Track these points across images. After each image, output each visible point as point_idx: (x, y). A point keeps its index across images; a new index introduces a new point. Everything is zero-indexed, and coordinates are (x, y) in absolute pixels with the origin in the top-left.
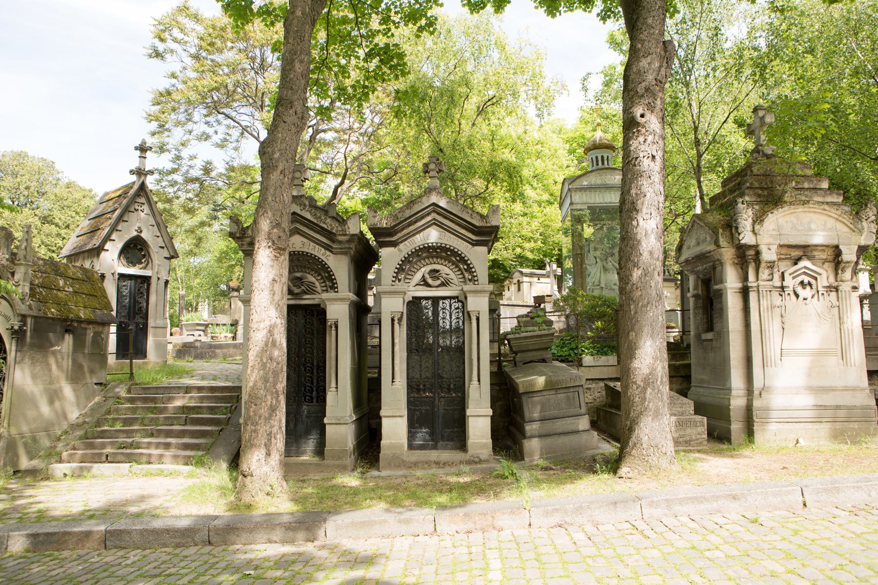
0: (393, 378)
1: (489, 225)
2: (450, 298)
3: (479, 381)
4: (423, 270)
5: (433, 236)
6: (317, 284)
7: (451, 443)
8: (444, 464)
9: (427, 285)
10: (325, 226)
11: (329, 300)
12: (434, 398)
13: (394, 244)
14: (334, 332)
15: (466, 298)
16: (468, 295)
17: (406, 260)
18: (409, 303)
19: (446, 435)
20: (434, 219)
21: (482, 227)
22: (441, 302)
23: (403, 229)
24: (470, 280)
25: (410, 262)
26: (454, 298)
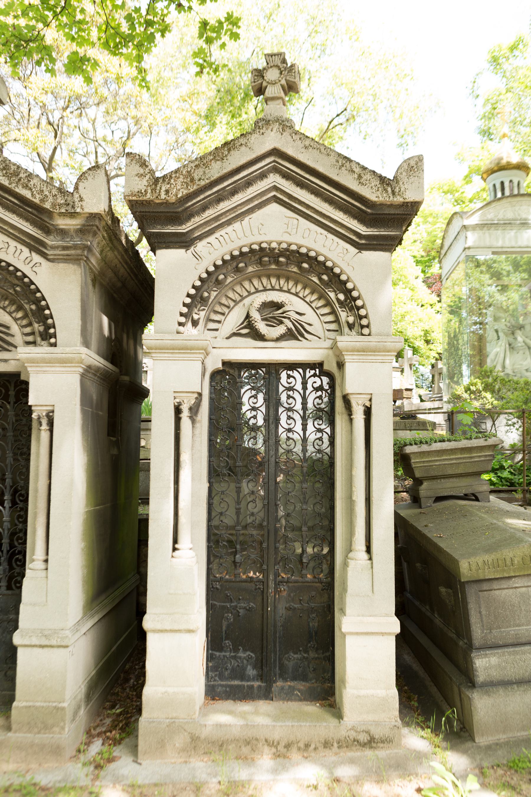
0: (175, 541)
1: (398, 200)
2: (305, 366)
3: (369, 550)
4: (247, 301)
5: (274, 227)
6: (15, 329)
7: (301, 685)
8: (288, 746)
9: (258, 336)
10: (27, 194)
11: (33, 361)
12: (264, 583)
13: (184, 242)
14: (45, 435)
15: (341, 365)
16: (348, 358)
17: (211, 279)
18: (215, 374)
19: (290, 665)
20: (275, 188)
21: (382, 205)
22: (284, 375)
23: (204, 208)
24: (351, 326)
25: (218, 282)
26: (312, 366)
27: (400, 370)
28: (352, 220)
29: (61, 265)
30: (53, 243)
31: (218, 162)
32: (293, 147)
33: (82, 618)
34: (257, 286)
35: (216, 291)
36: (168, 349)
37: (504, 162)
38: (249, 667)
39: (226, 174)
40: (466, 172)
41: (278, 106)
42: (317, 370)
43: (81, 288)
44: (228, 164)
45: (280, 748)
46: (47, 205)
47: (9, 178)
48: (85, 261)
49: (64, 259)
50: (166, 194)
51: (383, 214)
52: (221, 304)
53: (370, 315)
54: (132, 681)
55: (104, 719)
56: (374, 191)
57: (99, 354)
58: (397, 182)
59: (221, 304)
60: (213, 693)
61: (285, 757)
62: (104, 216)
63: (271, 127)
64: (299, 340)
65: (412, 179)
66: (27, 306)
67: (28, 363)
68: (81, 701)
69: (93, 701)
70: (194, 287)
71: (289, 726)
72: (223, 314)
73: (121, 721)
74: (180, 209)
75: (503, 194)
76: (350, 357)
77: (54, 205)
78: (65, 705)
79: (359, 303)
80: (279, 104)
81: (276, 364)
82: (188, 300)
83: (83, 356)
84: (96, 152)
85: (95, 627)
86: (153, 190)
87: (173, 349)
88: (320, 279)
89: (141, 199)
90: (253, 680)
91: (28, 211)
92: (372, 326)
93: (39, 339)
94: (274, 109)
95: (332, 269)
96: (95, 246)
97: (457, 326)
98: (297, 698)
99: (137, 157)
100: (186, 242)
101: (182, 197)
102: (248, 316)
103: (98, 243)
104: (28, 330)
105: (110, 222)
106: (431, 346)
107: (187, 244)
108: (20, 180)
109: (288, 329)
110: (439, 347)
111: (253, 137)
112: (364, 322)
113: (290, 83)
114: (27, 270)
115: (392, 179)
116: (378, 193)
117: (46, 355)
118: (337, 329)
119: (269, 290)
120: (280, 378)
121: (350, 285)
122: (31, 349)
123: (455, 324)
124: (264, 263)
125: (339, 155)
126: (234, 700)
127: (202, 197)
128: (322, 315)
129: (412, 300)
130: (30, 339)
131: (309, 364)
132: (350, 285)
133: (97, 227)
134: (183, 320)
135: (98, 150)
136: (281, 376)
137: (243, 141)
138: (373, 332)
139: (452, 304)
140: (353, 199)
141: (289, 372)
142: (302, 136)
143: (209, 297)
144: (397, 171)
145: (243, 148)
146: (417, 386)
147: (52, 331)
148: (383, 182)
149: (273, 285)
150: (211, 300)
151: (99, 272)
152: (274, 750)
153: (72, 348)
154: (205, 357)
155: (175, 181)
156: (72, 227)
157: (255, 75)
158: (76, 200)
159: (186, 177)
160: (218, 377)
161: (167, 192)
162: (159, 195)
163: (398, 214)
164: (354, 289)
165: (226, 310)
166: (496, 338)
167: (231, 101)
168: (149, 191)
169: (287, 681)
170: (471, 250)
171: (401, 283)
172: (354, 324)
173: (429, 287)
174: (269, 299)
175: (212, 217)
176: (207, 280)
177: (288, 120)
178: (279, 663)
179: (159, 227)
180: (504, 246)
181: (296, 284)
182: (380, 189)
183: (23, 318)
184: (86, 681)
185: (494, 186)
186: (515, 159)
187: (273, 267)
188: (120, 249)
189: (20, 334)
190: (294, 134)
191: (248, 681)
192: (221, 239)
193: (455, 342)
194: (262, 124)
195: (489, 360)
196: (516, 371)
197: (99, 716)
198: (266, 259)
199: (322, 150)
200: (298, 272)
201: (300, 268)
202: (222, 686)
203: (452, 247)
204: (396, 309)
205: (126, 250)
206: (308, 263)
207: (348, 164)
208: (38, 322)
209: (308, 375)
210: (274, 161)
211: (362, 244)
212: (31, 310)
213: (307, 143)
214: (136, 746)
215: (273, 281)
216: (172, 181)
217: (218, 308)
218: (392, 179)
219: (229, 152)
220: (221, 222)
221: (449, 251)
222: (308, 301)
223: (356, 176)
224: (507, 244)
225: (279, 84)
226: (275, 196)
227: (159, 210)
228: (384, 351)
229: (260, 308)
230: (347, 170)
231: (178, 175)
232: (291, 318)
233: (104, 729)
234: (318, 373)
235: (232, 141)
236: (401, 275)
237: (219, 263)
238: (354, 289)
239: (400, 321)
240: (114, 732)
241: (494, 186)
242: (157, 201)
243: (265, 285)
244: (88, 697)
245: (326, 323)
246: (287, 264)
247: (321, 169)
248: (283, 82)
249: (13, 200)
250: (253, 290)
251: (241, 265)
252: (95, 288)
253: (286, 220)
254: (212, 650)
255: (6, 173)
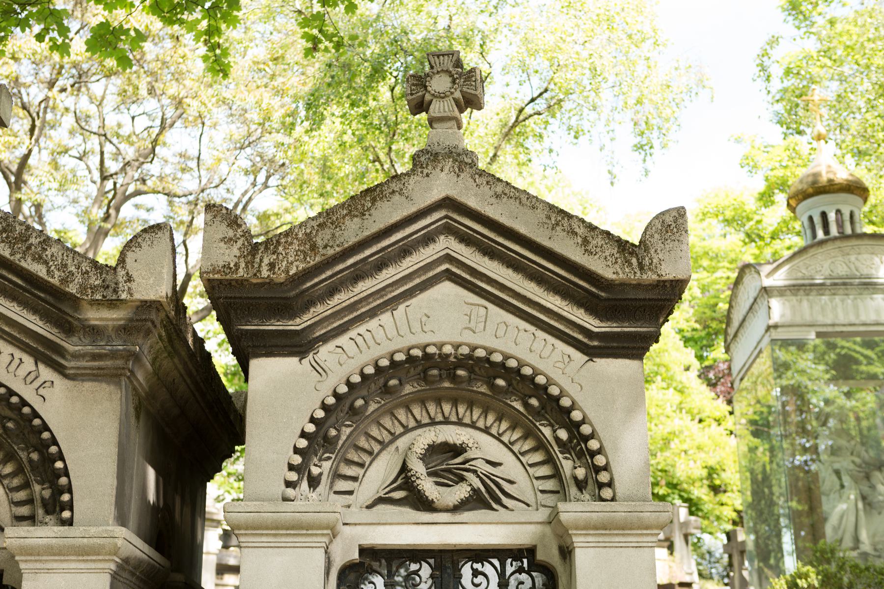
1: (650, 277)
2: (501, 553)
4: (402, 443)
5: (445, 318)
9: (421, 502)
10: (39, 270)
11: (31, 552)
13: (298, 345)
15: (566, 553)
16: (578, 540)
17: (342, 407)
21: (623, 285)
22: (466, 571)
23: (332, 291)
24: (581, 485)
25: (353, 412)
27: (667, 544)
28: (575, 308)
29: (88, 385)
30: (77, 348)
31: (355, 219)
32: (476, 195)
34: (418, 417)
35: (349, 426)
36: (267, 528)
37: (824, 179)
39: (368, 237)
40: (762, 187)
41: (450, 131)
42: (525, 561)
43: (120, 424)
44: (371, 222)
46: (72, 289)
47: (11, 246)
48: (129, 378)
49: (94, 375)
50: (270, 270)
51: (625, 300)
52: (358, 448)
53: (613, 466)
56: (609, 263)
57: (139, 535)
58: (647, 250)
59: (358, 448)
62: (165, 305)
63: (441, 165)
64: (493, 509)
65: (670, 245)
66: (23, 455)
67: (21, 555)
70: (312, 420)
72: (361, 465)
74: (292, 294)
75: (827, 232)
76: (582, 539)
77: (83, 288)
79: (594, 444)
80: (451, 128)
81: (452, 551)
82: (303, 443)
83: (120, 542)
84: (102, 153)
86: (249, 264)
87: (277, 528)
88: (526, 405)
89: (228, 277)
91: (39, 298)
92: (617, 484)
93: (40, 512)
94: (444, 134)
95: (545, 388)
96: (146, 353)
97: (767, 459)
99: (224, 211)
100: (301, 346)
101: (295, 274)
102: (404, 468)
103: (151, 347)
104: (21, 495)
105: (173, 313)
106: (723, 497)
107: (302, 349)
108: (29, 248)
109: (473, 489)
110: (736, 500)
111: (413, 180)
112: (604, 477)
113: (467, 96)
114: (28, 393)
115: (637, 244)
116: (617, 266)
117: (54, 541)
118: (558, 488)
119: (440, 423)
120: (460, 577)
121: (576, 415)
122: (24, 530)
123: (763, 455)
124: (431, 379)
125: (552, 207)
127: (329, 273)
128: (531, 465)
129: (681, 409)
130: (24, 511)
131: (511, 550)
132: (576, 415)
133: (153, 322)
134: (293, 476)
135: (106, 150)
136: (463, 571)
137: (395, 186)
138: (619, 495)
139: (757, 418)
140: (576, 275)
141: (475, 566)
142: (490, 179)
143: (338, 437)
144: (645, 232)
145: (396, 198)
146: (701, 575)
147: (66, 497)
148: (624, 250)
149: (447, 414)
150: (341, 442)
151: (146, 393)
153: (101, 528)
154: (331, 542)
155: (285, 248)
156: (110, 323)
157: (413, 85)
158: (121, 279)
159: (302, 243)
160: (352, 577)
161: (272, 266)
162: (259, 271)
163: (650, 300)
164: (583, 422)
165: (367, 459)
166: (838, 487)
167: (350, 80)
168: (243, 265)
170: (779, 330)
171: (659, 378)
172: (585, 481)
173: (712, 385)
174: (440, 439)
175: (344, 305)
176: (336, 409)
177: (466, 153)
179: (256, 322)
180: (837, 322)
181: (485, 413)
182: (619, 261)
183: (13, 475)
185: (811, 219)
186: (842, 175)
187: (447, 384)
188: (183, 353)
189: (6, 503)
190: (477, 176)
192: (359, 340)
193: (766, 490)
194: (424, 161)
195: (829, 530)
196: (880, 547)
198: (435, 372)
199: (524, 200)
200: (490, 393)
201: (492, 386)
203: (746, 323)
204: (653, 427)
205: (192, 355)
206: (504, 379)
207: (565, 222)
208: (41, 483)
209: (509, 570)
210: (446, 217)
211: (594, 347)
212: (30, 461)
213: (499, 189)
215: (447, 408)
216: (281, 248)
217: (353, 456)
218: (637, 244)
219: (373, 204)
220: (359, 312)
221: (742, 331)
222: (506, 441)
223: (580, 240)
224: (842, 319)
225: (451, 98)
226: (447, 270)
227: (258, 295)
228: (639, 528)
229: (424, 455)
230: (564, 230)
231: (289, 239)
232: (479, 470)
234: (525, 565)
235: (377, 186)
236: (659, 365)
237: (356, 379)
238: (583, 422)
239: (661, 450)
241: (811, 219)
242: (254, 281)
243: (432, 415)
245: (537, 478)
246: (470, 380)
247: (523, 230)
248: (458, 95)
249: (15, 279)
250: (412, 424)
251: (393, 382)
252: (138, 421)
253: (467, 309)
255: (7, 237)
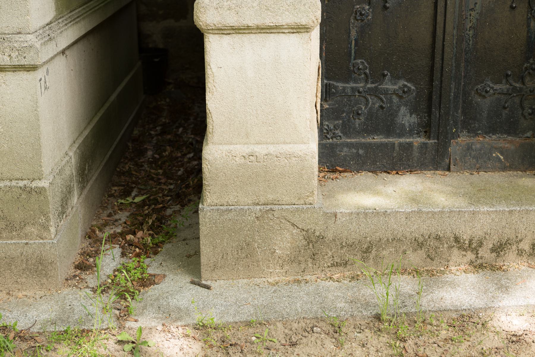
7: (506, 142)
19: (485, 104)
33: (56, 19)
38: (403, 110)
45: (485, 253)
54: (150, 153)
55: (115, 213)
60: (334, 160)
61: (493, 268)
68: (71, 176)
69: (91, 182)
71: (503, 212)
73: (148, 215)
78: (44, 184)
85: (80, 46)
90: (411, 133)
98: (498, 164)
126: (374, 172)
152: (470, 256)
169: (477, 135)
178: (464, 102)
184: (77, 145)
191: (400, 136)
197: (104, 208)
202: (350, 146)
214: (197, 253)
233: (119, 230)
240: (140, 234)
244: (83, 174)
254: (327, 78)
